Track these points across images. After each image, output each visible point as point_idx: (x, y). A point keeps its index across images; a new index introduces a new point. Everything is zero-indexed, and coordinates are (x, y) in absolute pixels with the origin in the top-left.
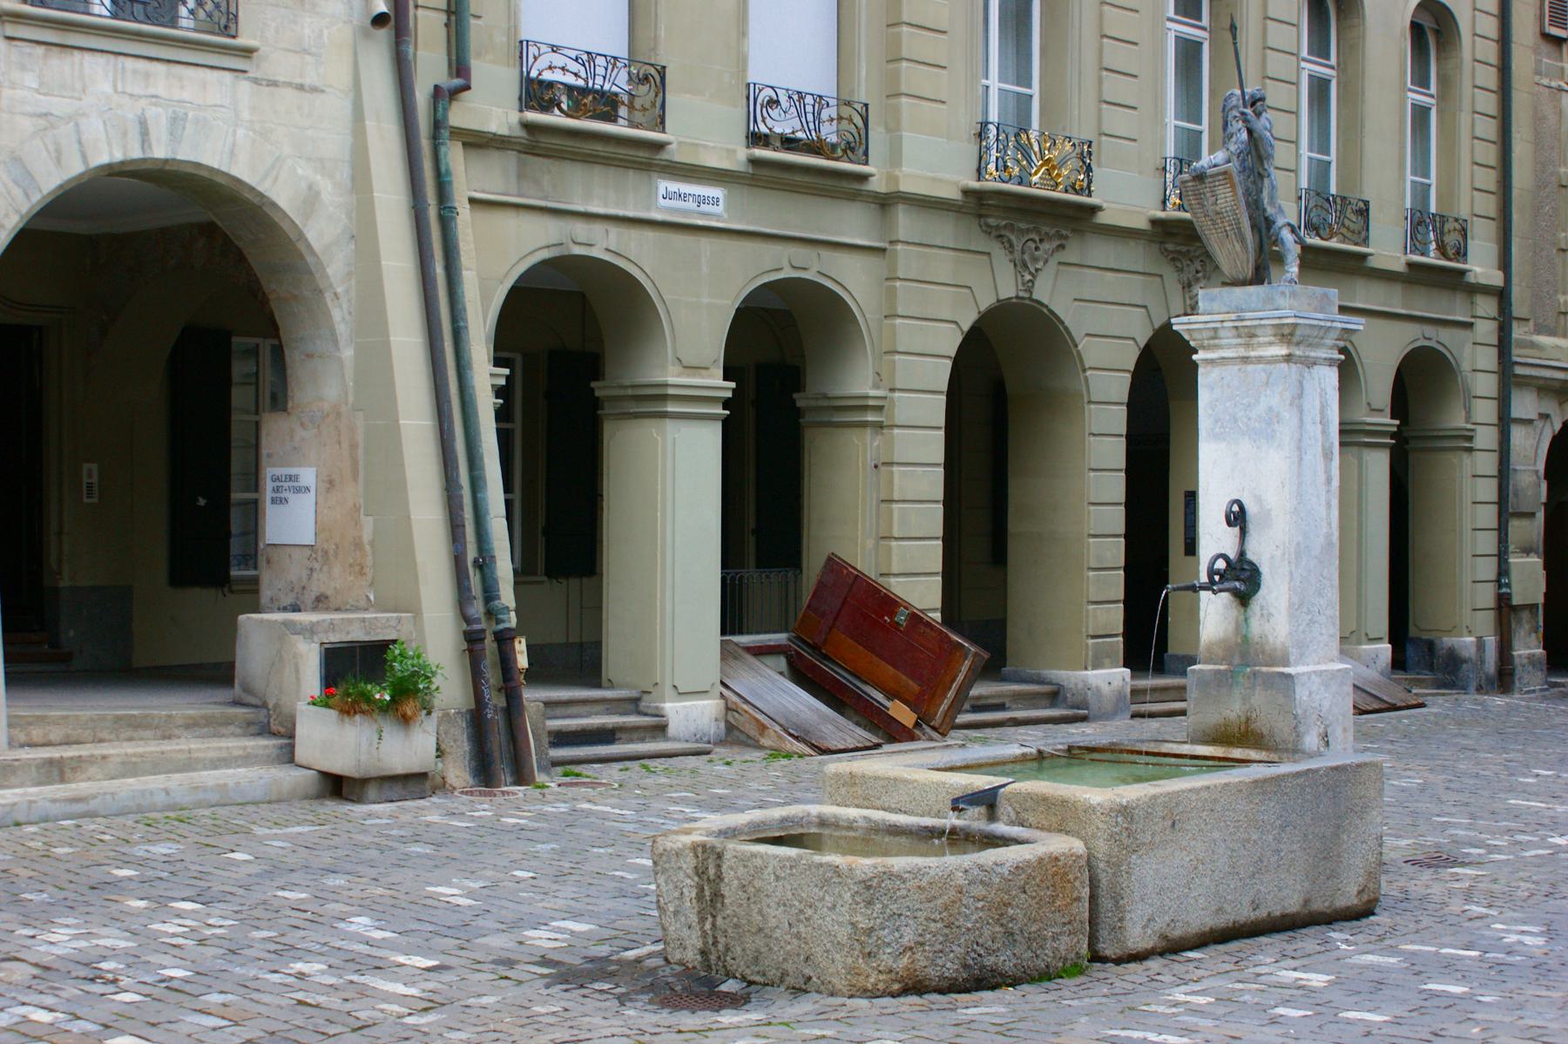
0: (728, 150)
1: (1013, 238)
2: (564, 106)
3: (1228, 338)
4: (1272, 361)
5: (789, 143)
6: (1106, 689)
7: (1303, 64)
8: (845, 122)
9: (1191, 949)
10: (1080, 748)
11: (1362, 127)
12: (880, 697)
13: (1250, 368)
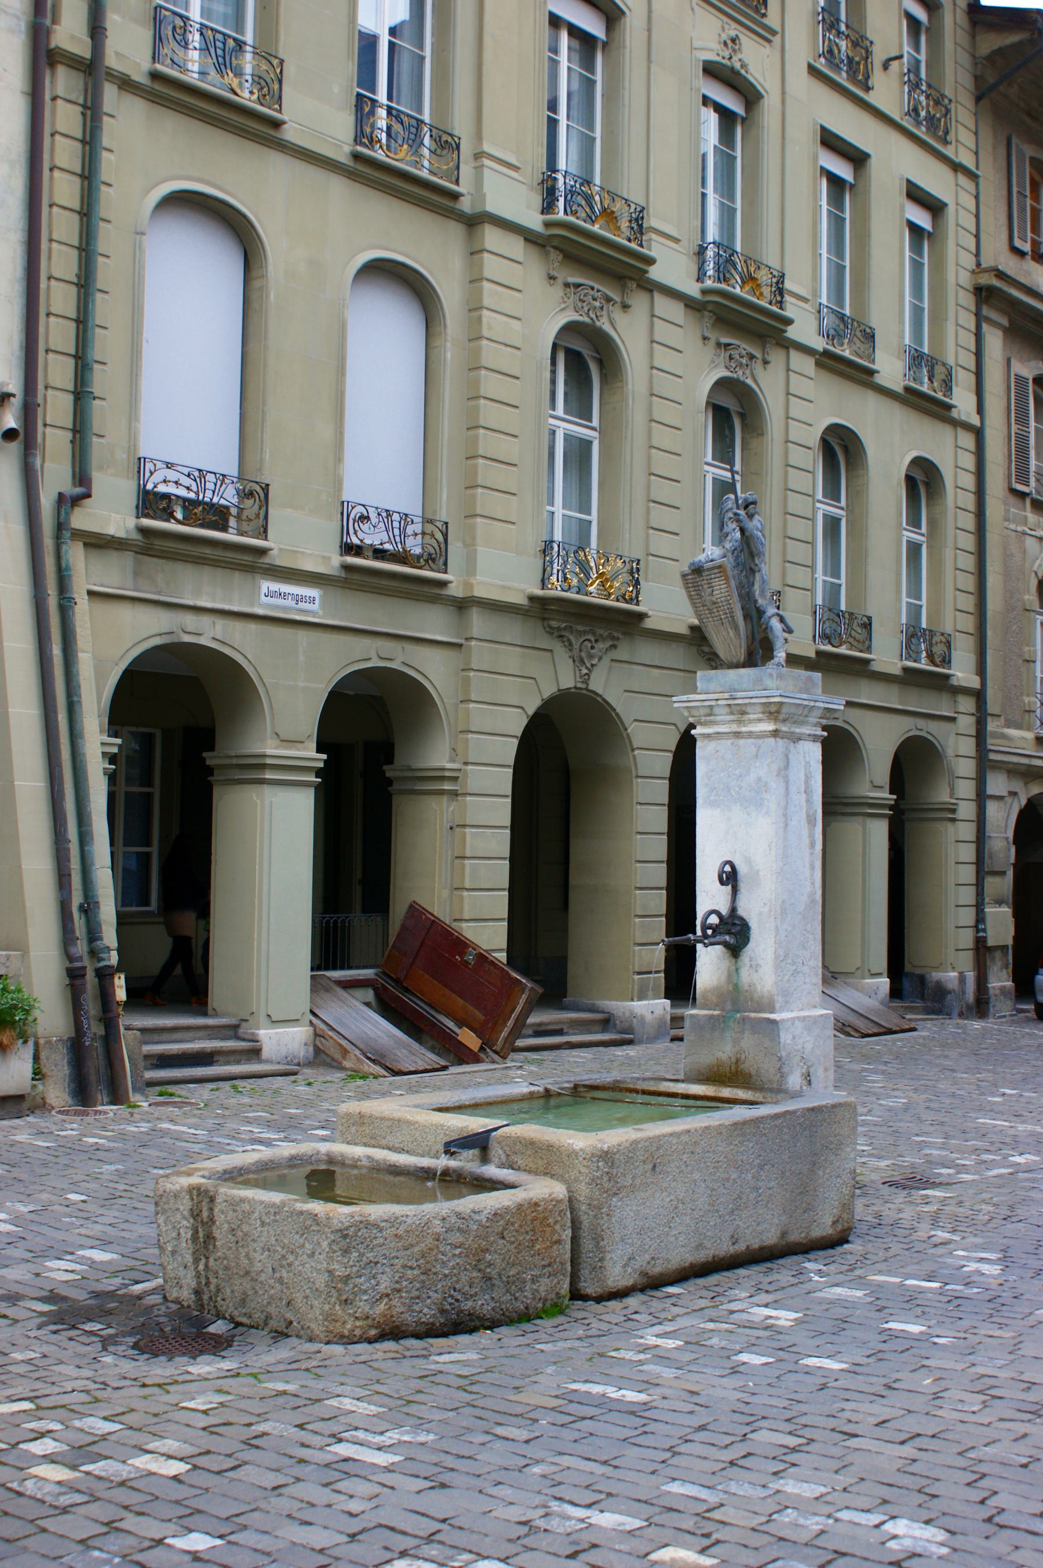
0: (323, 557)
1: (572, 638)
4: (761, 735)
5: (379, 553)
6: (649, 1017)
7: (818, 505)
8: (427, 537)
9: (671, 1283)
10: (585, 1086)
12: (451, 1024)
13: (742, 742)
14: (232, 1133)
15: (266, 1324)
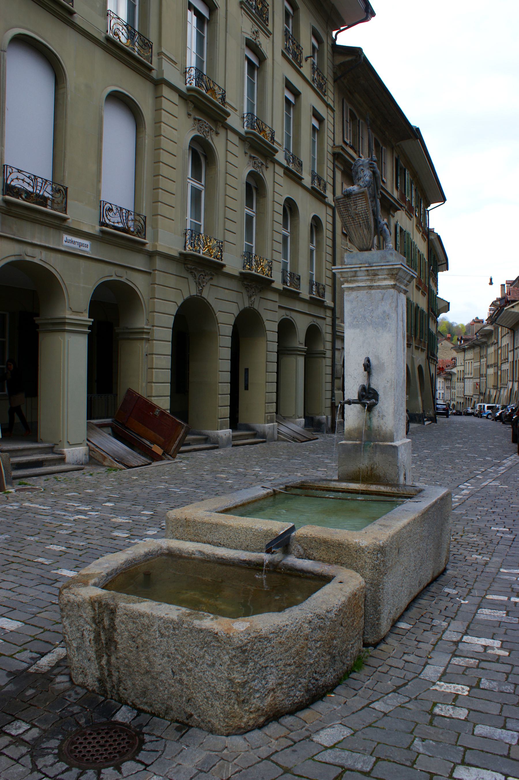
0: (92, 226)
1: (196, 273)
2: (23, 197)
3: (362, 276)
4: (386, 287)
6: (224, 437)
11: (298, 252)
13: (373, 291)
14: (63, 507)
15: (167, 714)
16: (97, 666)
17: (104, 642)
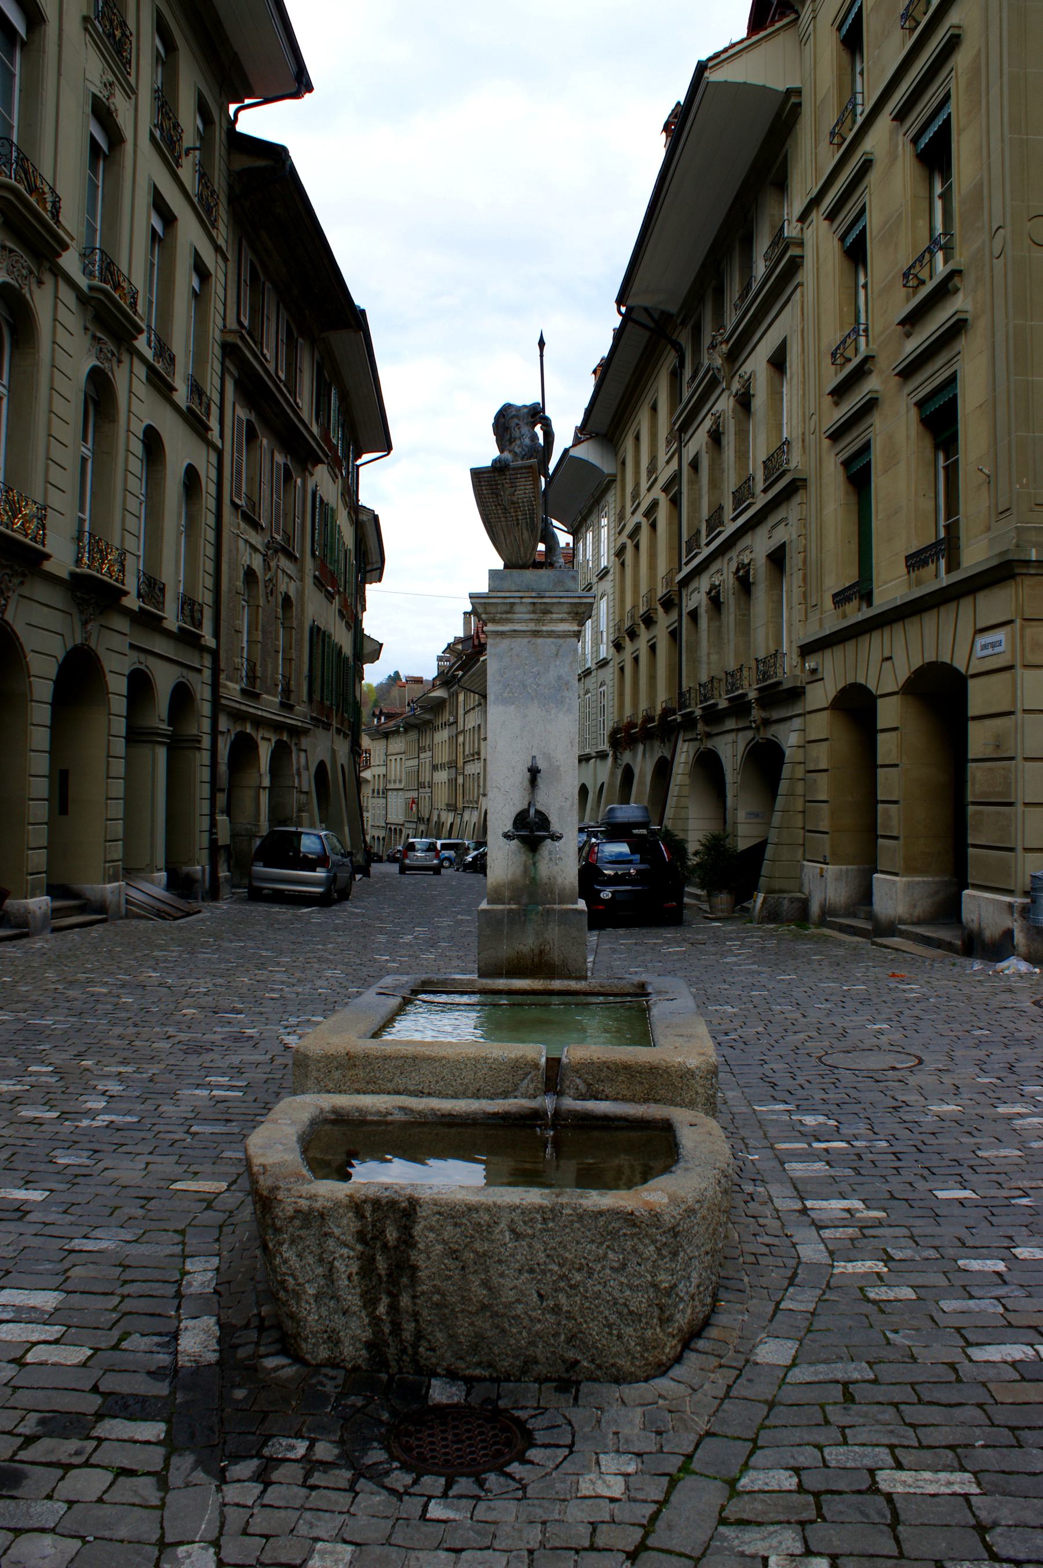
3: (522, 612)
6: (38, 912)
13: (540, 641)
16: (367, 1321)
17: (383, 1272)
